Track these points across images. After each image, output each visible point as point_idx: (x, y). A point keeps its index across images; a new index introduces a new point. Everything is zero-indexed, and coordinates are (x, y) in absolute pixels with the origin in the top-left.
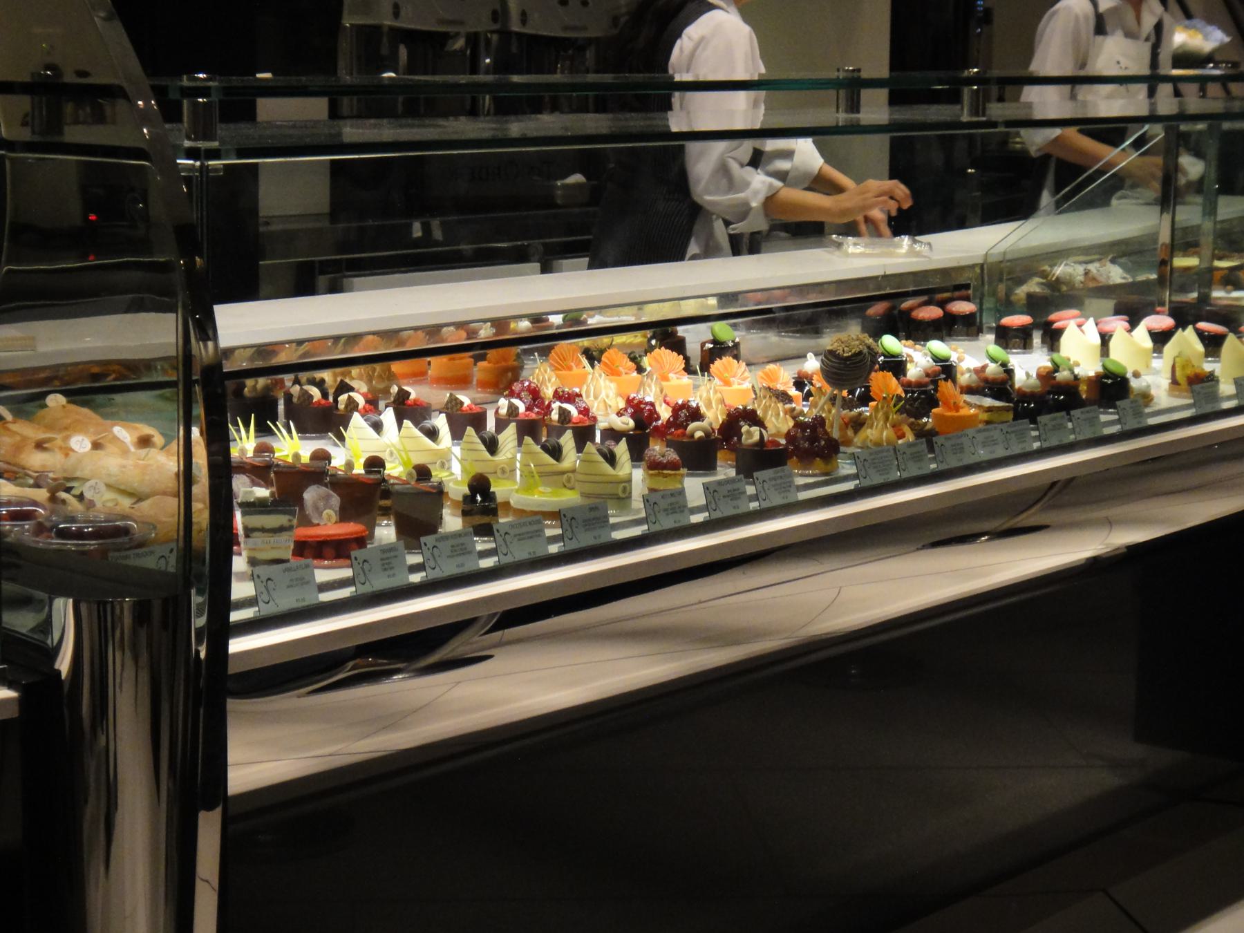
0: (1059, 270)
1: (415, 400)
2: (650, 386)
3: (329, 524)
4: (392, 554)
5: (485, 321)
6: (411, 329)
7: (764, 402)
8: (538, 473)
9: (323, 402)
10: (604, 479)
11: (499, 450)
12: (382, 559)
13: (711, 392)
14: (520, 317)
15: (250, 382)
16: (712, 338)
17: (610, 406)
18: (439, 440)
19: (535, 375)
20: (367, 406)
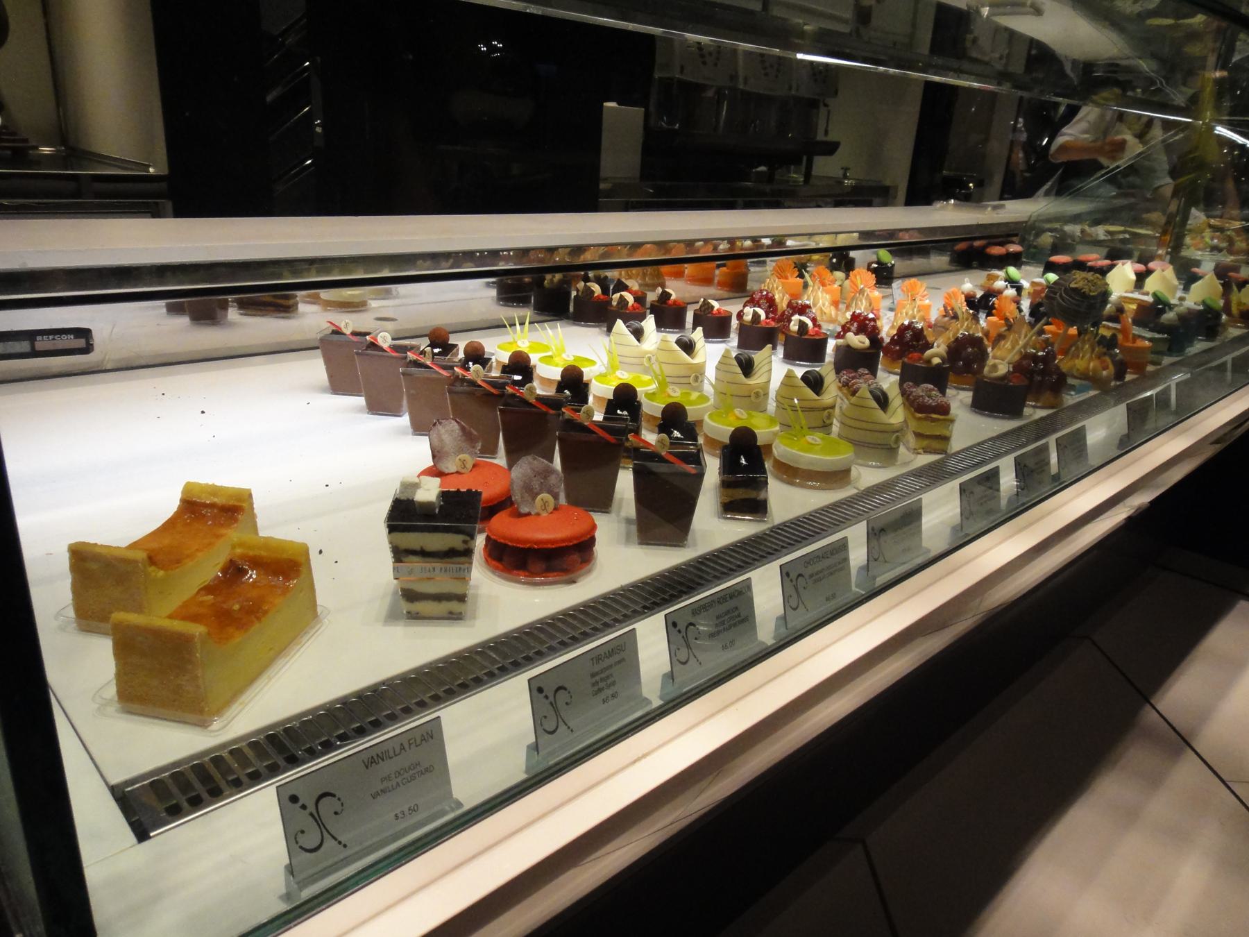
0: (1068, 228)
1: (675, 301)
2: (861, 301)
3: (544, 514)
4: (617, 658)
5: (723, 239)
6: (674, 241)
7: (966, 324)
8: (800, 407)
9: (602, 297)
10: (878, 427)
11: (754, 372)
12: (593, 675)
13: (915, 310)
14: (746, 238)
15: (548, 277)
16: (876, 260)
17: (825, 313)
18: (695, 353)
19: (766, 284)
20: (636, 305)
